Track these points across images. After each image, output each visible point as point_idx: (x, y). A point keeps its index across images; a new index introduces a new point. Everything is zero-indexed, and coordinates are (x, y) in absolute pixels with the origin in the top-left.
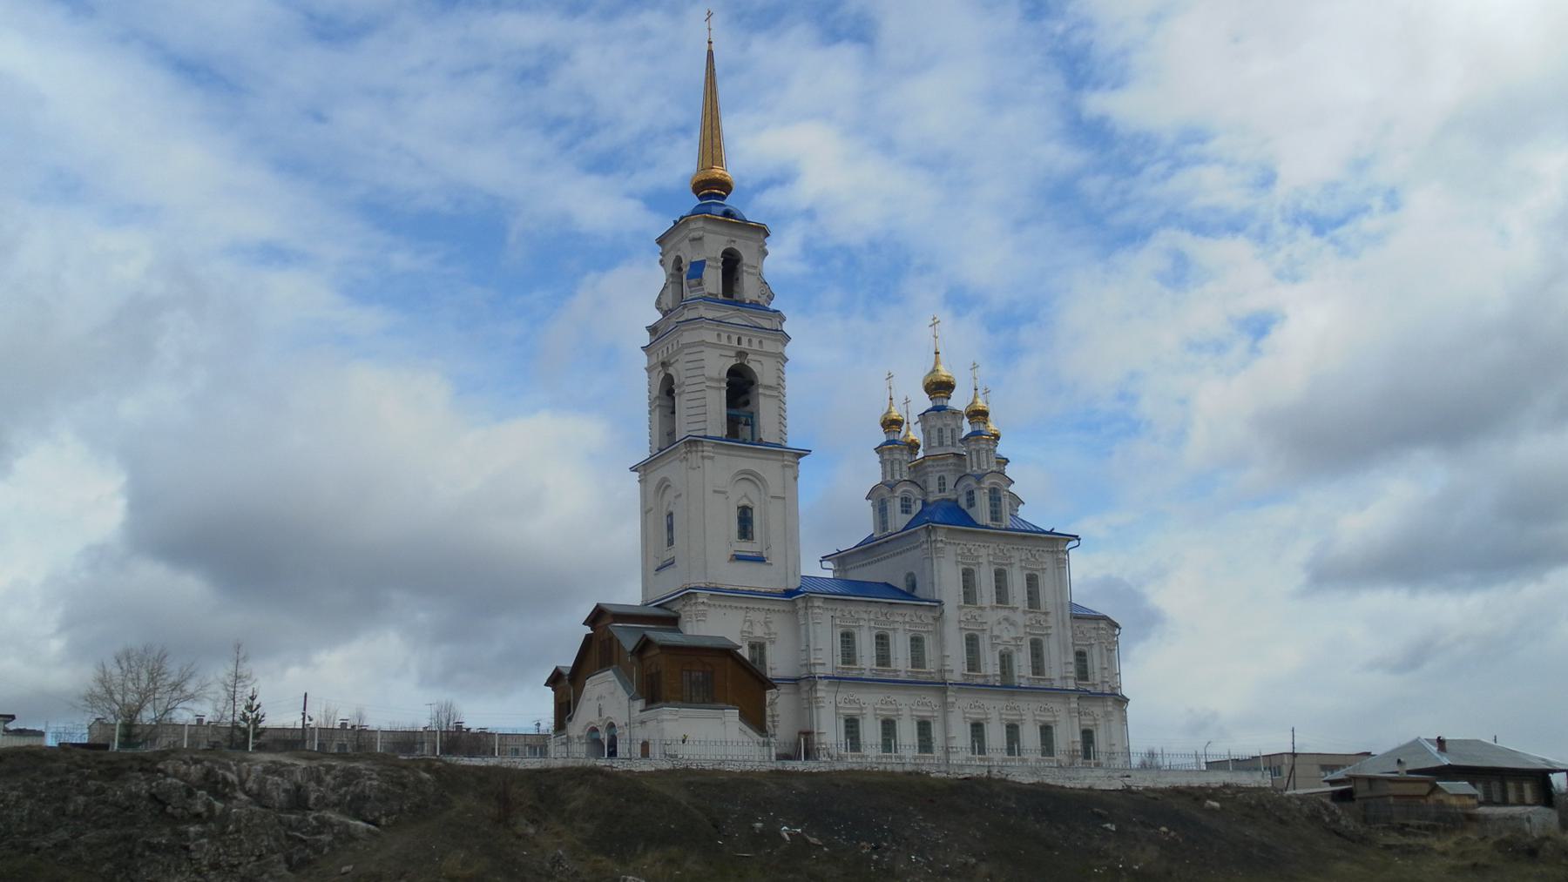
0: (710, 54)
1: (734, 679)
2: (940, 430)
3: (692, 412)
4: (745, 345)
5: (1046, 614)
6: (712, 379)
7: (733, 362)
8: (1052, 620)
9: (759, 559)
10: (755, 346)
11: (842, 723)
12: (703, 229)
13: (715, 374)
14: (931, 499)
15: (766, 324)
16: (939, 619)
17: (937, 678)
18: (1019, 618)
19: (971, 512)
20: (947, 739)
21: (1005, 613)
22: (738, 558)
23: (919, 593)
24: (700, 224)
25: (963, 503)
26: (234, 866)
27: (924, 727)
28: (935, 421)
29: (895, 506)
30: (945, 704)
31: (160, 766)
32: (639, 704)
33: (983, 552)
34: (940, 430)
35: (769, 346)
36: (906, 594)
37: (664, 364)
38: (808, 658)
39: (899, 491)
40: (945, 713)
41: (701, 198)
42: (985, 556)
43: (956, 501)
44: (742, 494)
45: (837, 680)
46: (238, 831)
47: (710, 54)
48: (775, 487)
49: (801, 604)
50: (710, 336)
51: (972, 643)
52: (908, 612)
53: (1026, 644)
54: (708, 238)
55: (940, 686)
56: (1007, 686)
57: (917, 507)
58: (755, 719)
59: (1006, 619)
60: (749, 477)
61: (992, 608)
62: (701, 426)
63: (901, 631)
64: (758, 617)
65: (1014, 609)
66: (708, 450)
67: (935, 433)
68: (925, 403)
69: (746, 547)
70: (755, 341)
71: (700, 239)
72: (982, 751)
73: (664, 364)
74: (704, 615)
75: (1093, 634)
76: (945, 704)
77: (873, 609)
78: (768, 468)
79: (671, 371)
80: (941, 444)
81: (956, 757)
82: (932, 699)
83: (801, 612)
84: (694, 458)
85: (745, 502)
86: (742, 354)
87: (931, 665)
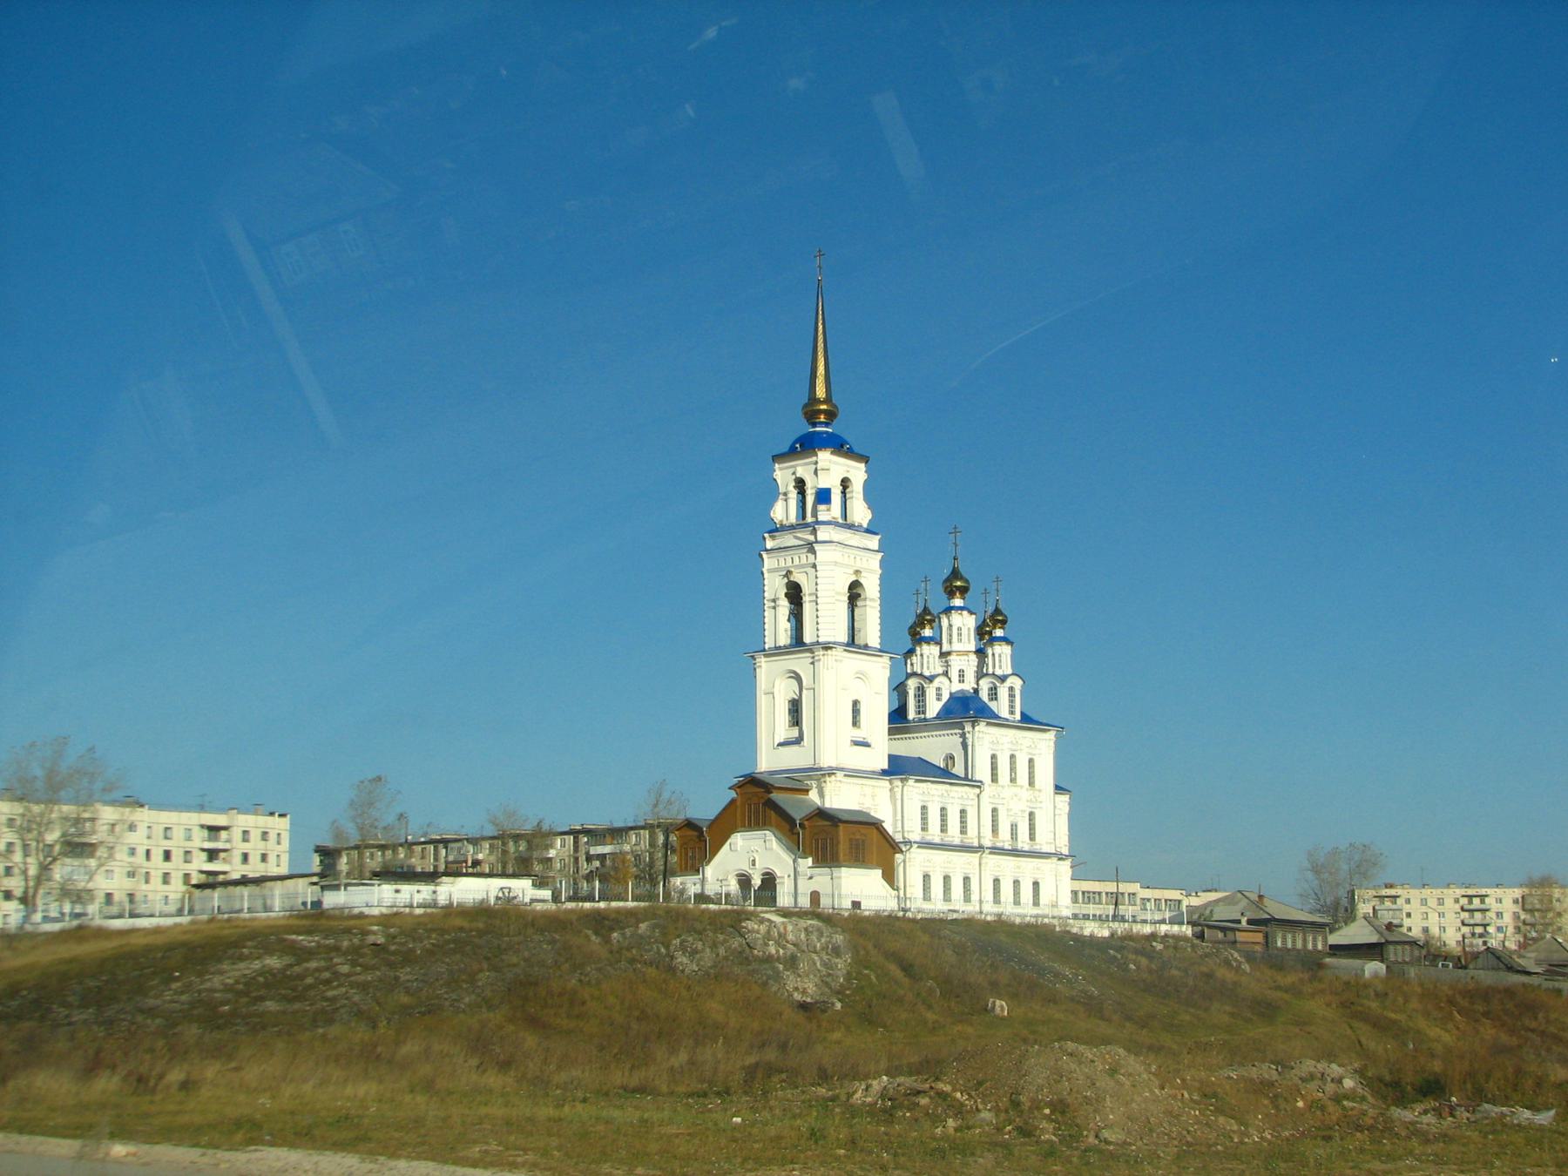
19: (993, 705)
21: (1015, 790)
22: (856, 743)
25: (984, 695)
58: (889, 877)
69: (859, 734)
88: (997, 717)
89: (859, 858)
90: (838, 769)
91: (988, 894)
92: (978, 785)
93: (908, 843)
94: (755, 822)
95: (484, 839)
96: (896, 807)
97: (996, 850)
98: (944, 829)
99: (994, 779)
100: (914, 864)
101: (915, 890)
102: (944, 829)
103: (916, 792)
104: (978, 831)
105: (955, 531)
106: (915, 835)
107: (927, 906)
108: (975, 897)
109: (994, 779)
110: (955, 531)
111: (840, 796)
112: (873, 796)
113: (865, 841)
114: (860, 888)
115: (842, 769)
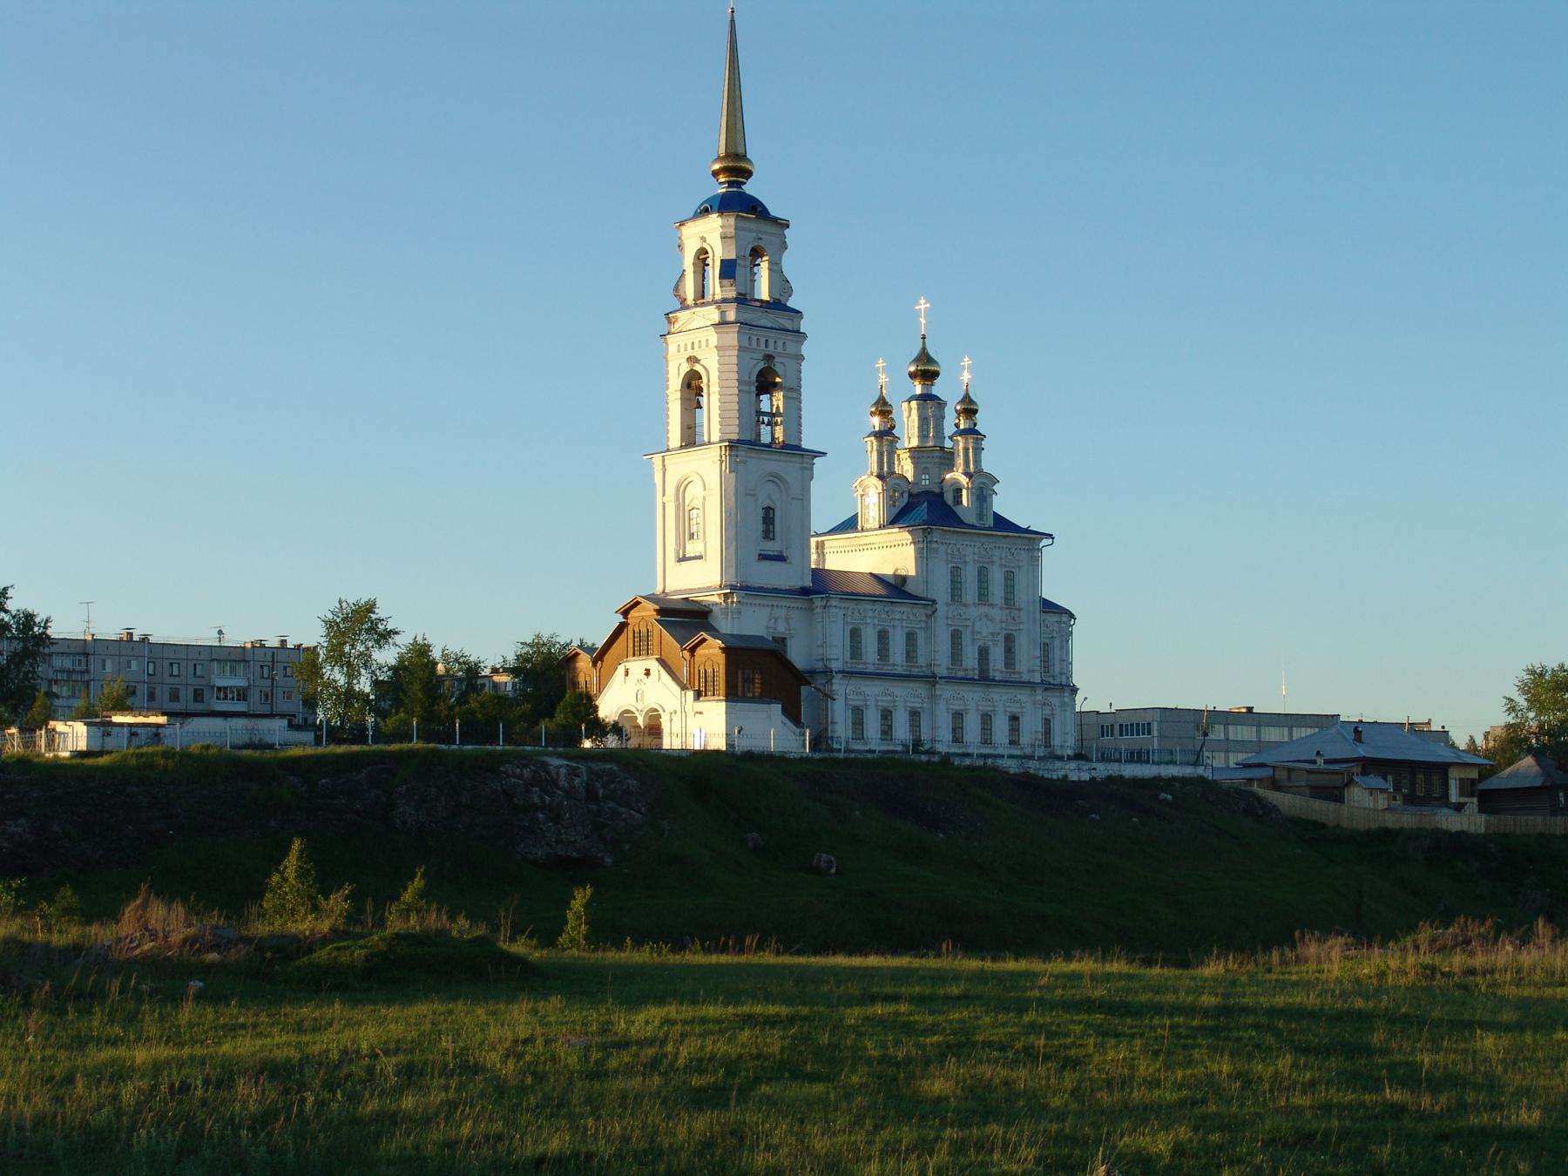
7: (761, 365)
8: (1023, 615)
9: (780, 558)
15: (788, 325)
17: (927, 671)
18: (997, 614)
21: (985, 609)
22: (764, 557)
45: (849, 674)
51: (956, 637)
53: (1001, 638)
56: (984, 679)
58: (792, 714)
64: (781, 613)
69: (771, 547)
82: (921, 689)
83: (819, 610)
85: (768, 503)
86: (769, 358)
98: (883, 652)
102: (883, 652)
106: (838, 655)
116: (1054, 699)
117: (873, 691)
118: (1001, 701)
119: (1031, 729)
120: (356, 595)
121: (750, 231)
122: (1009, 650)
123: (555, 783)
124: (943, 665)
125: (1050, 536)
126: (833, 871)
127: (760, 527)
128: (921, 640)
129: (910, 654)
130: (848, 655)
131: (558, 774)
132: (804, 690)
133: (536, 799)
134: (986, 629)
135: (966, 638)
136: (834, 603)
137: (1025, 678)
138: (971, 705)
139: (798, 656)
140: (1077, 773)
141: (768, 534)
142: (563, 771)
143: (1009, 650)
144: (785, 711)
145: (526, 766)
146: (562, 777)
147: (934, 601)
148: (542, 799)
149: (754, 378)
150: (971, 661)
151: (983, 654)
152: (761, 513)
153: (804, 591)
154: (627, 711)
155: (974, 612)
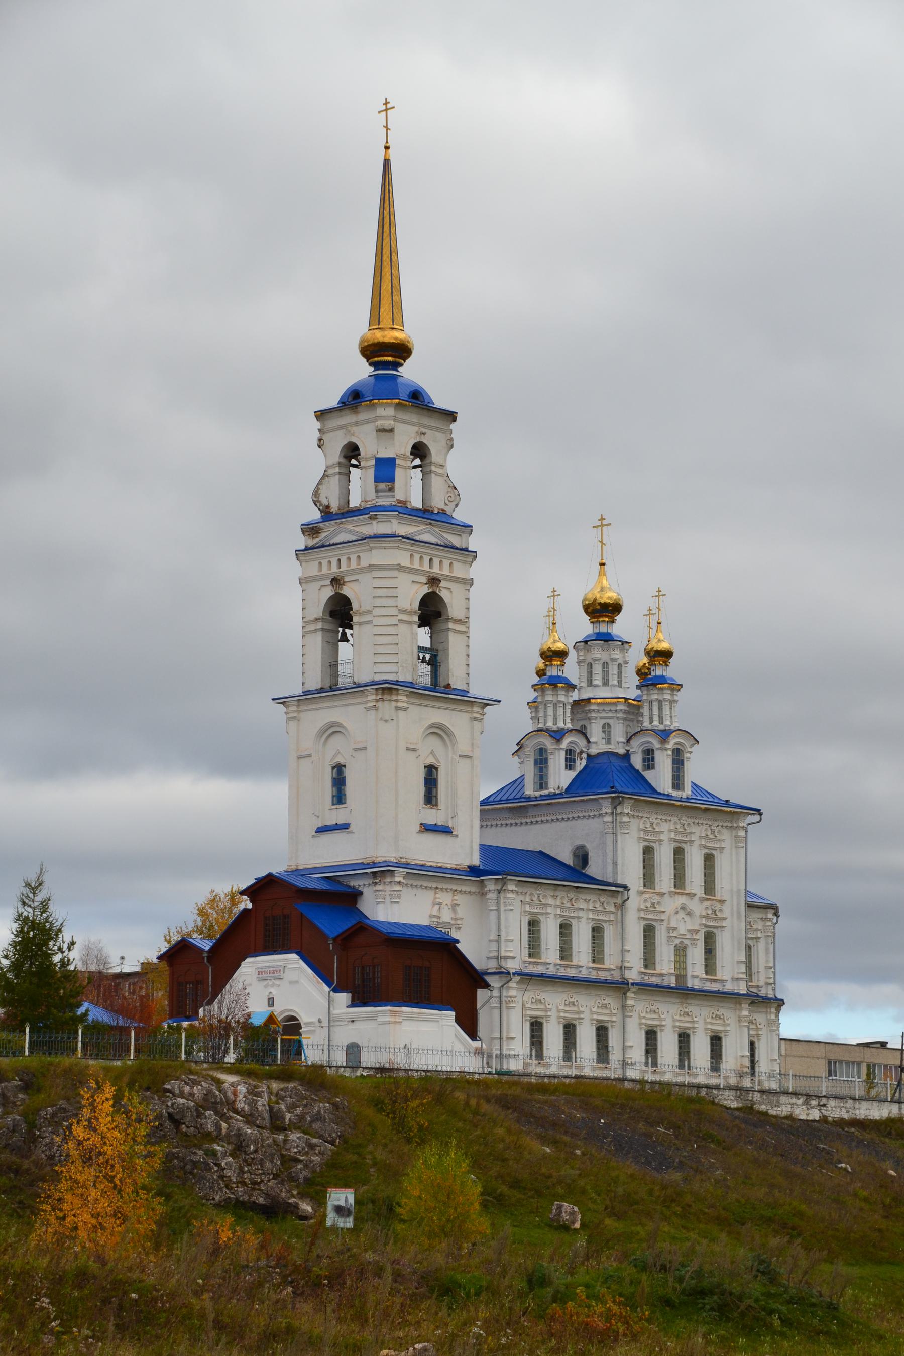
0: (387, 163)
1: (435, 973)
2: (605, 665)
3: (381, 650)
4: (436, 569)
5: (722, 902)
6: (403, 611)
7: (425, 590)
8: (727, 911)
9: (445, 830)
10: (446, 571)
11: (527, 1026)
12: (395, 419)
13: (406, 605)
14: (594, 751)
15: (455, 541)
16: (621, 906)
17: (616, 976)
18: (697, 908)
19: (648, 775)
20: (624, 1048)
21: (681, 900)
22: (427, 828)
23: (593, 870)
24: (390, 411)
25: (637, 761)
26: (255, 1183)
27: (602, 1032)
28: (598, 653)
29: (557, 761)
30: (624, 1007)
31: (167, 1086)
32: (343, 998)
33: (665, 827)
34: (605, 665)
35: (459, 571)
36: (575, 873)
37: (336, 581)
38: (498, 951)
39: (565, 744)
40: (624, 1017)
41: (376, 365)
42: (667, 829)
43: (627, 756)
44: (431, 751)
45: (528, 978)
46: (256, 1151)
47: (387, 163)
48: (463, 747)
49: (491, 886)
50: (402, 557)
51: (649, 932)
52: (592, 897)
53: (701, 936)
54: (399, 428)
55: (620, 987)
56: (682, 992)
57: (580, 765)
58: (469, 1024)
59: (683, 908)
60: (438, 731)
61: (672, 894)
62: (393, 668)
63: (584, 920)
64: (445, 898)
65: (691, 896)
66: (402, 699)
67: (598, 669)
68: (585, 627)
69: (432, 816)
70: (446, 563)
71: (391, 431)
72: (655, 1064)
73: (336, 581)
74: (399, 897)
75: (759, 925)
76: (624, 1007)
77: (560, 893)
78: (456, 720)
79: (346, 591)
80: (606, 683)
81: (629, 1061)
82: (611, 1001)
83: (492, 896)
84: (387, 708)
85: (431, 761)
86: (434, 581)
87: (611, 961)
88: (654, 791)
89: (420, 995)
90: (398, 865)
91: (637, 1054)
92: (615, 890)
93: (503, 973)
94: (273, 944)
95: (802, 1095)
96: (489, 929)
97: (647, 989)
98: (565, 952)
99: (649, 878)
100: (508, 1016)
101: (518, 1046)
102: (565, 952)
103: (514, 907)
104: (626, 954)
105: (602, 524)
106: (516, 954)
107: (537, 1069)
108: (615, 1056)
109: (649, 878)
110: (602, 524)
111: (397, 908)
112: (340, 613)
113: (435, 973)
114: (421, 1039)
115: (407, 866)
116: (760, 1018)
117: (555, 1005)
118: (702, 1020)
119: (734, 1053)
120: (538, 654)
121: (413, 424)
122: (710, 951)
123: (231, 1105)
124: (635, 972)
125: (758, 811)
126: (577, 1225)
127: (421, 789)
128: (609, 933)
129: (597, 955)
130: (525, 952)
131: (235, 1094)
132: (482, 994)
133: (210, 1127)
134: (684, 925)
135: (661, 936)
136: (511, 887)
137: (729, 987)
138: (668, 1022)
139: (472, 948)
140: (784, 1108)
141: (430, 798)
142: (242, 1089)
143: (710, 951)
144: (458, 1021)
145: (195, 1083)
146: (241, 1097)
147: (625, 887)
148: (218, 1128)
149: (416, 605)
150: (665, 965)
151: (680, 952)
152: (422, 773)
153: (473, 871)
154: (293, 1018)
155: (670, 905)
